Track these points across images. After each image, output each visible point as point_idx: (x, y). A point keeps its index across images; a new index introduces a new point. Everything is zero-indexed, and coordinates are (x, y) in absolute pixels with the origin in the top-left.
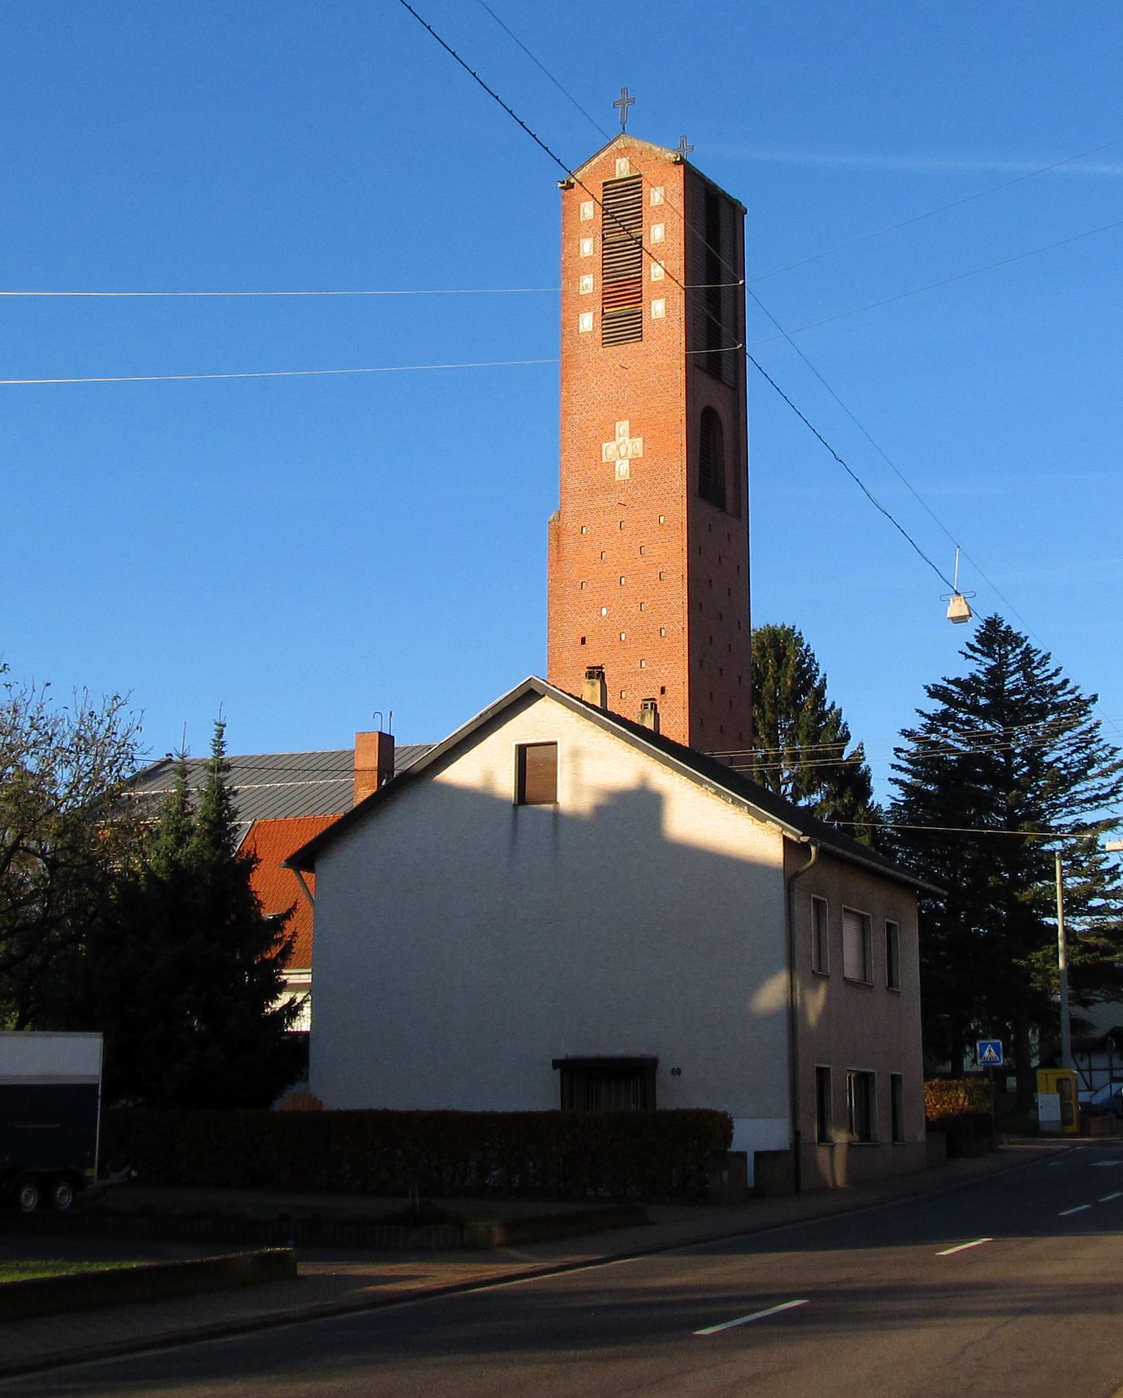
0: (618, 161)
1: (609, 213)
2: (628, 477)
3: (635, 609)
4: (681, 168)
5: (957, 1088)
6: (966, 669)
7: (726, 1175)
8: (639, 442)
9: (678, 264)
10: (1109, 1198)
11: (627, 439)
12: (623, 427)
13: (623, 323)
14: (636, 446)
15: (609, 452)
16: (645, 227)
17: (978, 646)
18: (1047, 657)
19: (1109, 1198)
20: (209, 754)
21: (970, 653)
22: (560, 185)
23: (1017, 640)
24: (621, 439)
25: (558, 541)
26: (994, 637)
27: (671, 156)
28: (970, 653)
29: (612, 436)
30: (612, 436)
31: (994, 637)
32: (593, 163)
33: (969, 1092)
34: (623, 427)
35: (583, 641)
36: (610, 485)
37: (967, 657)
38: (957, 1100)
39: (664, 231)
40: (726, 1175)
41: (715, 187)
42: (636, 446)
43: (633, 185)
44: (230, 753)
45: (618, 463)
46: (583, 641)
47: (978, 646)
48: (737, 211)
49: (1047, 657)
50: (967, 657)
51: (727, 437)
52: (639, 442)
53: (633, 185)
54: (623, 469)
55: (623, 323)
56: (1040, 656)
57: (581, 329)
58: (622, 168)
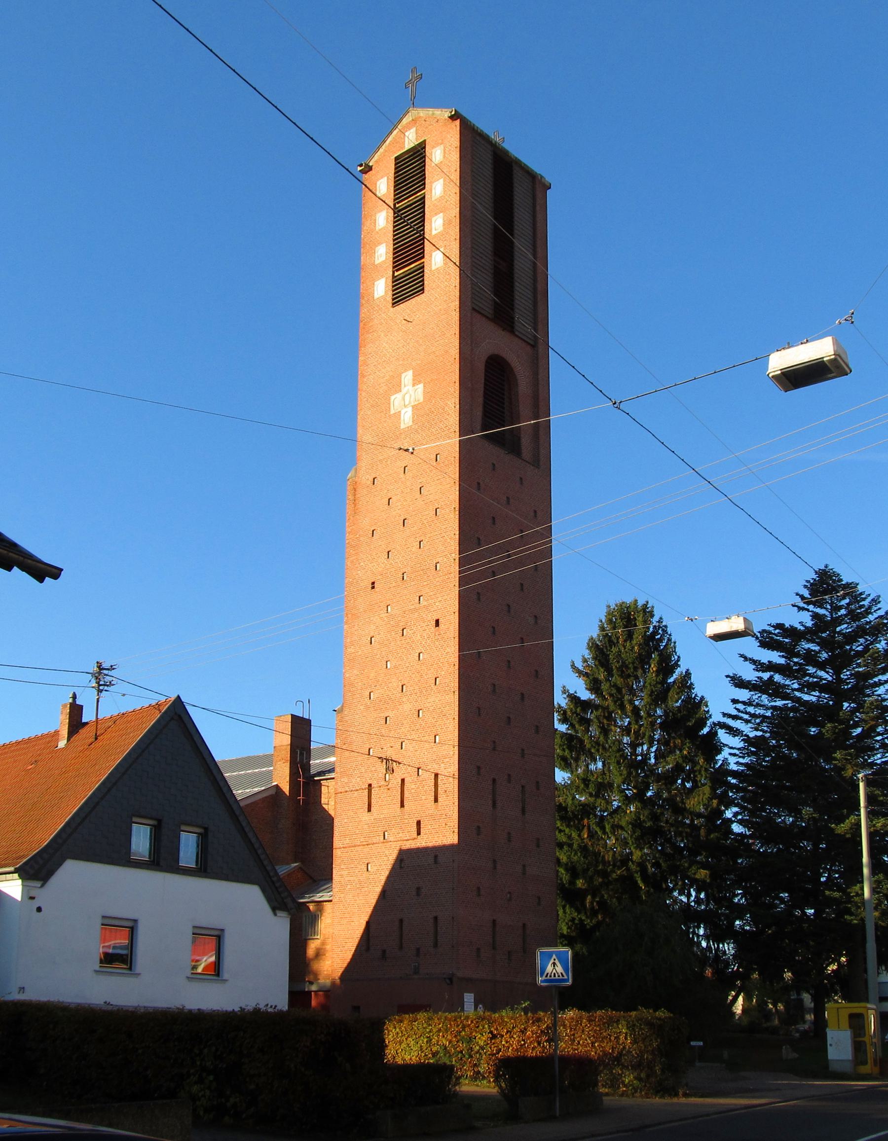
2: (411, 423)
4: (458, 122)
5: (618, 1022)
6: (802, 619)
8: (420, 387)
9: (454, 211)
10: (882, 1133)
11: (410, 387)
12: (407, 377)
13: (408, 284)
15: (396, 404)
18: (876, 601)
19: (882, 1133)
20: (94, 719)
22: (359, 169)
23: (850, 589)
24: (406, 389)
25: (355, 495)
26: (824, 585)
27: (446, 114)
28: (802, 605)
31: (824, 585)
32: (388, 142)
33: (631, 1027)
34: (407, 377)
38: (617, 1038)
39: (442, 191)
41: (506, 153)
43: (418, 154)
44: (100, 717)
45: (403, 412)
48: (538, 186)
49: (876, 601)
50: (800, 609)
51: (523, 386)
52: (420, 387)
53: (418, 154)
54: (407, 418)
55: (408, 284)
56: (869, 599)
57: (376, 296)
58: (410, 140)
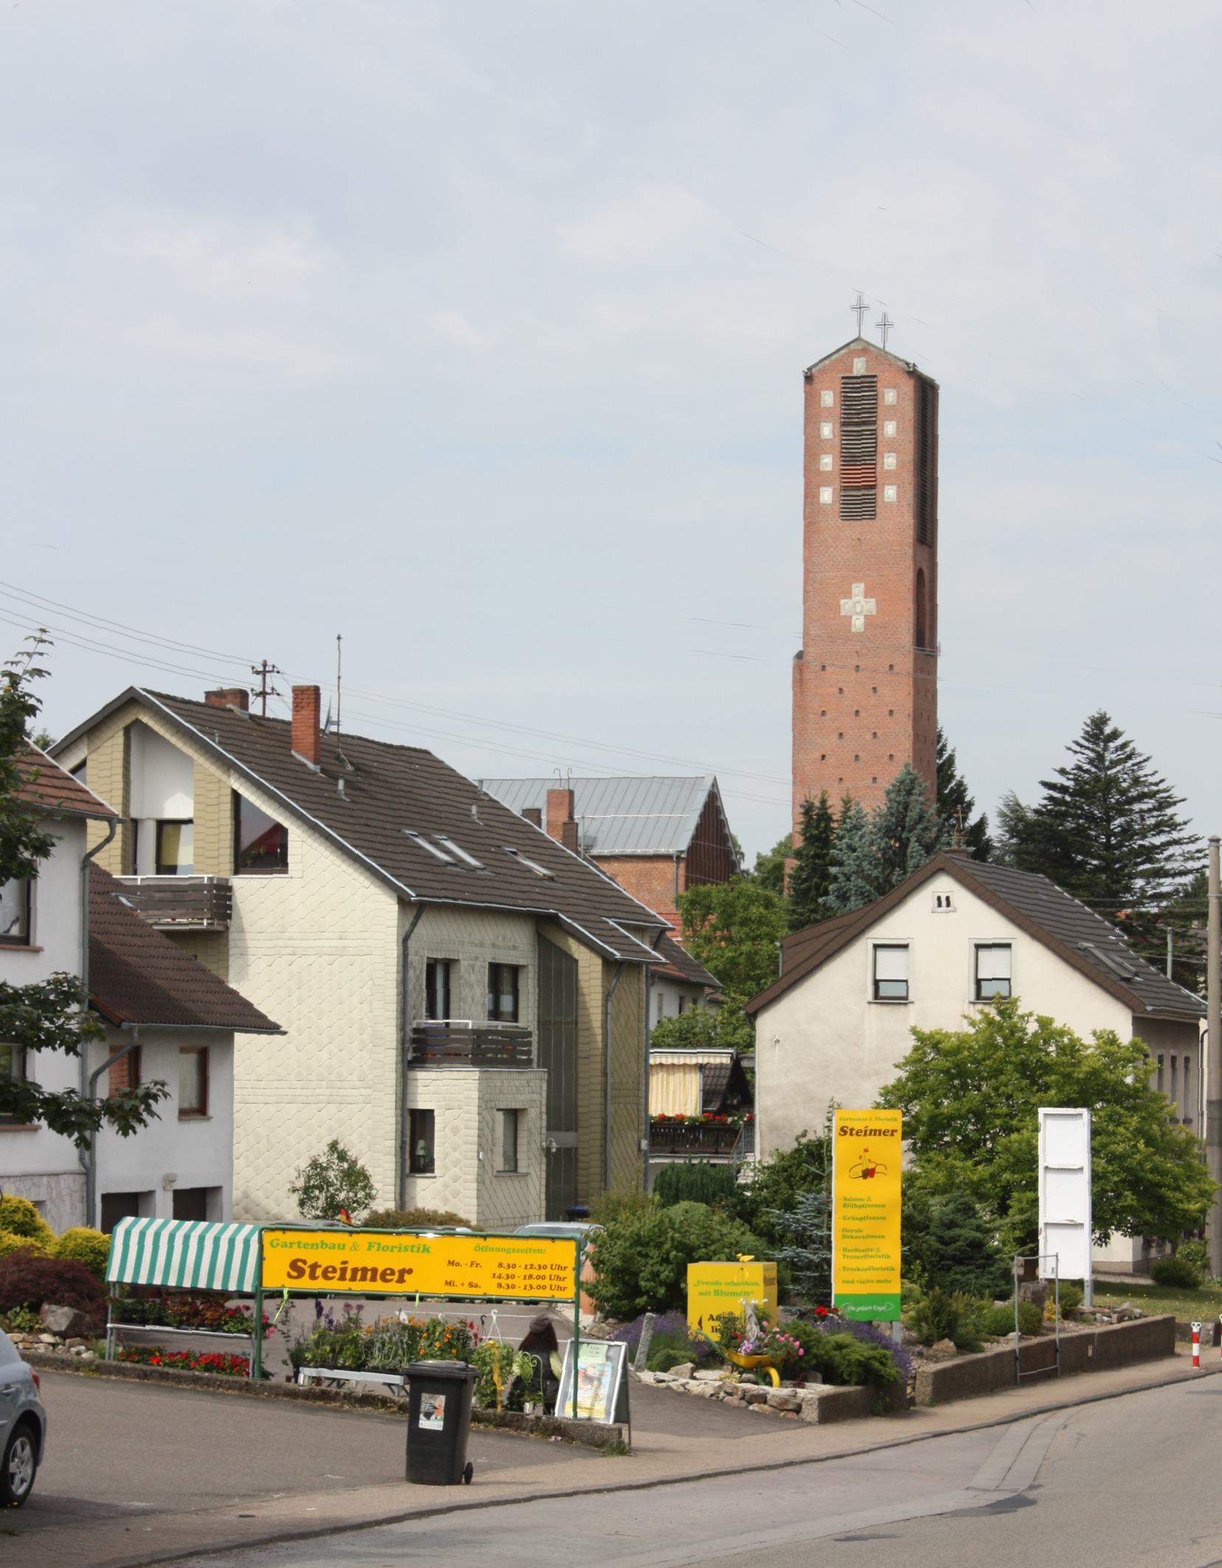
0: (856, 360)
1: (848, 402)
3: (869, 737)
7: (1090, 1353)
8: (873, 601)
12: (858, 589)
14: (870, 605)
16: (879, 456)
17: (1086, 743)
18: (1047, 785)
21: (1078, 749)
29: (848, 594)
30: (848, 594)
34: (858, 589)
35: (823, 757)
36: (848, 636)
37: (1076, 752)
40: (1090, 1353)
42: (870, 605)
45: (854, 618)
46: (823, 757)
47: (1086, 743)
50: (1076, 752)
52: (873, 601)
54: (858, 624)
